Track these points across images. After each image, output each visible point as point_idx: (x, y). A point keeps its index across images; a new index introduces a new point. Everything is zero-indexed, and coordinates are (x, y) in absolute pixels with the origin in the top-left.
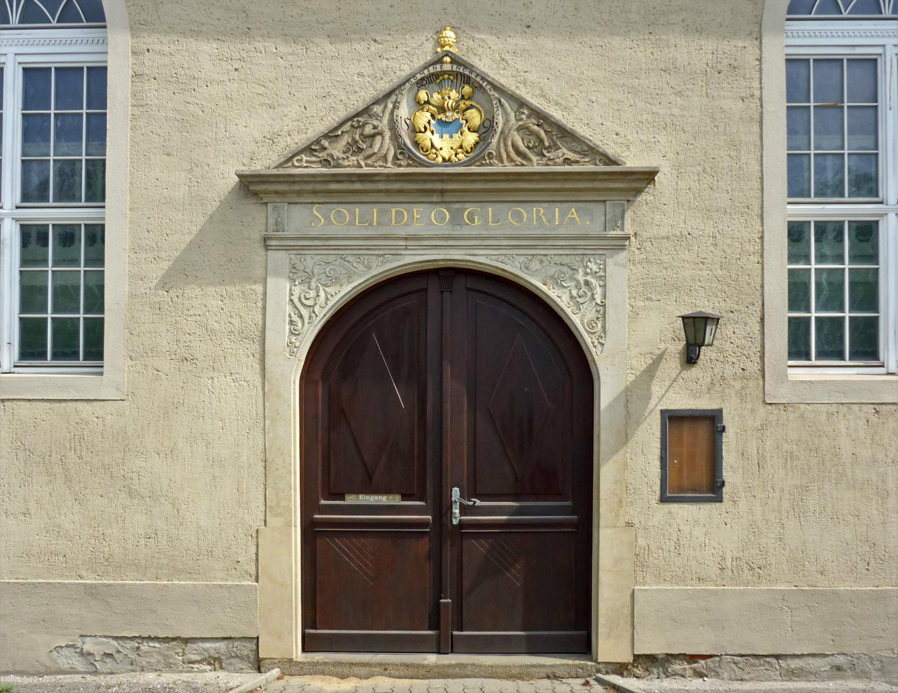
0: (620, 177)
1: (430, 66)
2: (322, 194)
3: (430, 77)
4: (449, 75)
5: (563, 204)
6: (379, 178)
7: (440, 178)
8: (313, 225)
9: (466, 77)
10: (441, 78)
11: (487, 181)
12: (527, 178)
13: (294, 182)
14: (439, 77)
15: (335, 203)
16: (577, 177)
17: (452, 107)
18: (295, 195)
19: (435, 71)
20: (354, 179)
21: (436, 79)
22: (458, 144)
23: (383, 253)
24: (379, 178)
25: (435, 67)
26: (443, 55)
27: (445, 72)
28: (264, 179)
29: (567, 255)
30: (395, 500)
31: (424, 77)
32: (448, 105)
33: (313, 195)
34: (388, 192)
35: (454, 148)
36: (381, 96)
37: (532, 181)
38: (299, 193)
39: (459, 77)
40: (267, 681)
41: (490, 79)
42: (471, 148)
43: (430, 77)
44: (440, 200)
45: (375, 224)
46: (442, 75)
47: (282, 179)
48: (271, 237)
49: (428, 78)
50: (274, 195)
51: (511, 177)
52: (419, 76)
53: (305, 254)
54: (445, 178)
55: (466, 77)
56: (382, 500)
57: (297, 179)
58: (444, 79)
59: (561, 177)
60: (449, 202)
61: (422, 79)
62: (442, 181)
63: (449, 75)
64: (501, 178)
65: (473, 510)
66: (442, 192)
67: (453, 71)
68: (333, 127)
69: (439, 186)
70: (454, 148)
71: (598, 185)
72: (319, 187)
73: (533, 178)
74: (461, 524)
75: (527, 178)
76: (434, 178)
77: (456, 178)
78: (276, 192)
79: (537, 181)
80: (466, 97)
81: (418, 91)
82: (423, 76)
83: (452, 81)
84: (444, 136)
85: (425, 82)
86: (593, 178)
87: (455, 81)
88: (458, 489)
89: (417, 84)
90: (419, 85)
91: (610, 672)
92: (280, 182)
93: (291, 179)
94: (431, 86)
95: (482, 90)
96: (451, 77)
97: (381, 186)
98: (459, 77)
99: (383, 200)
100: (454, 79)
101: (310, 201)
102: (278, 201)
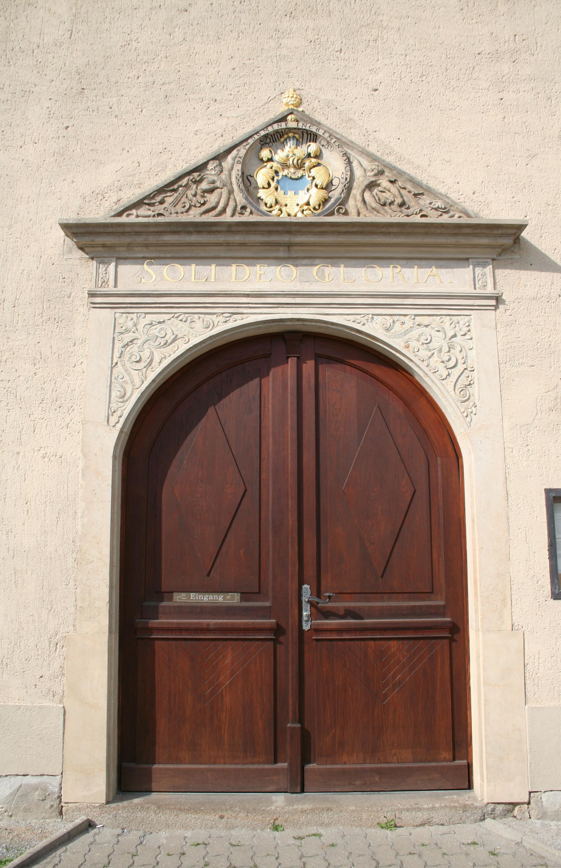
0: (485, 231)
1: (274, 123)
2: (154, 248)
3: (274, 135)
4: (294, 133)
5: (423, 261)
6: (219, 229)
7: (287, 228)
8: (143, 281)
9: (312, 136)
10: (285, 136)
11: (339, 233)
12: (383, 230)
13: (123, 233)
14: (283, 135)
15: (169, 258)
16: (439, 231)
17: (298, 164)
18: (125, 249)
19: (280, 128)
20: (191, 229)
21: (281, 137)
22: (305, 201)
23: (222, 311)
24: (219, 229)
25: (279, 124)
26: (288, 113)
27: (290, 130)
28: (90, 230)
29: (429, 315)
30: (233, 599)
31: (268, 134)
32: (293, 162)
33: (144, 249)
34: (228, 244)
35: (300, 204)
36: (222, 151)
37: (389, 234)
38: (129, 246)
39: (305, 135)
40: (69, 835)
41: (338, 136)
42: (319, 205)
43: (274, 135)
44: (287, 255)
45: (213, 280)
46: (287, 134)
47: (110, 230)
48: (96, 294)
49: (271, 135)
50: (101, 249)
51: (366, 229)
52: (263, 133)
53: (133, 313)
54: (293, 229)
55: (312, 136)
56: (219, 598)
57: (128, 229)
58: (289, 137)
59: (422, 230)
60: (297, 258)
61: (266, 136)
62: (289, 233)
63: (294, 133)
64: (355, 229)
65: (327, 614)
66: (289, 246)
67: (299, 129)
68: (169, 181)
69: (286, 238)
70: (300, 204)
71: (462, 240)
72: (152, 239)
73: (391, 230)
74: (316, 630)
75: (383, 230)
76: (280, 229)
77: (305, 229)
78: (104, 246)
79: (396, 234)
80: (312, 155)
81: (261, 149)
82: (267, 132)
83: (297, 140)
84: (289, 193)
85: (268, 140)
86: (455, 232)
87: (301, 140)
88: (309, 587)
89: (261, 141)
90: (263, 143)
91: (347, 763)
92: (108, 234)
93: (120, 230)
94: (275, 144)
95: (329, 148)
96: (297, 136)
97: (221, 238)
98: (305, 135)
99: (223, 255)
100: (300, 137)
101: (141, 255)
102: (106, 256)
